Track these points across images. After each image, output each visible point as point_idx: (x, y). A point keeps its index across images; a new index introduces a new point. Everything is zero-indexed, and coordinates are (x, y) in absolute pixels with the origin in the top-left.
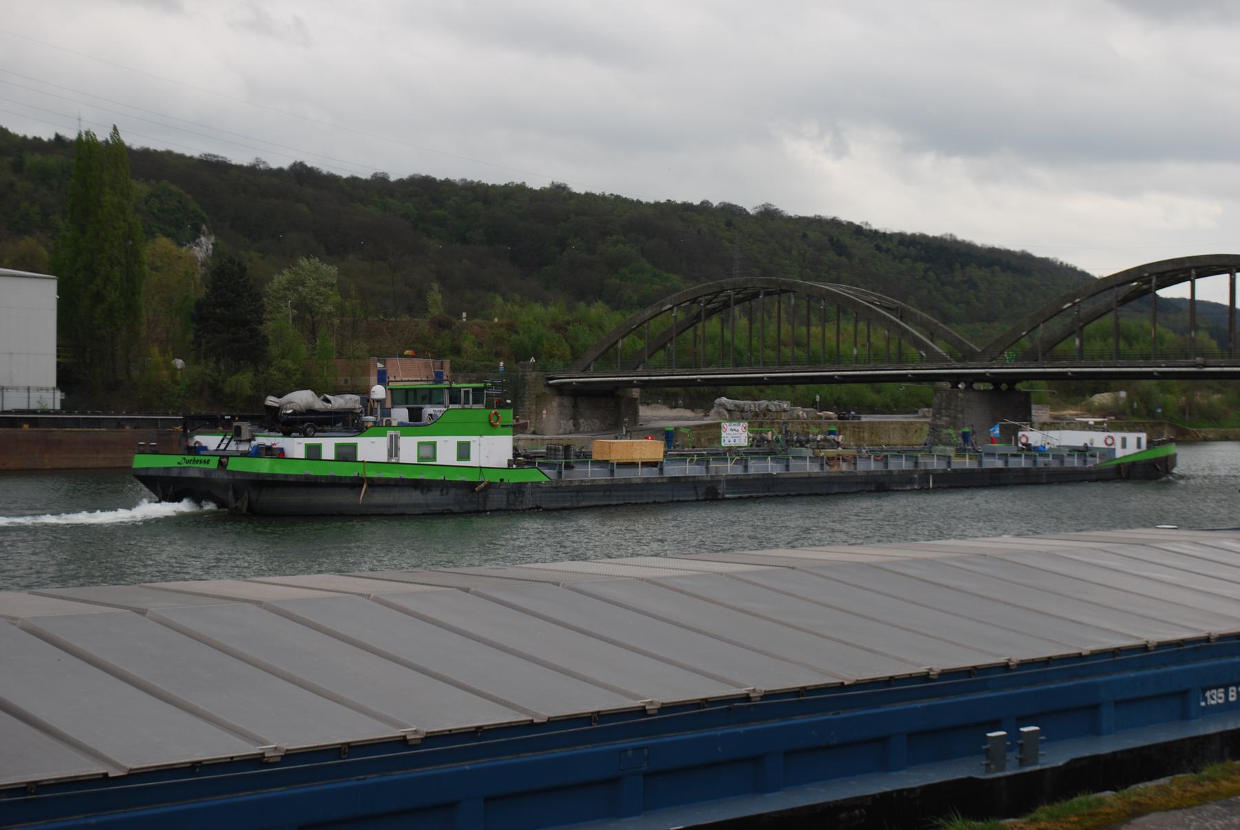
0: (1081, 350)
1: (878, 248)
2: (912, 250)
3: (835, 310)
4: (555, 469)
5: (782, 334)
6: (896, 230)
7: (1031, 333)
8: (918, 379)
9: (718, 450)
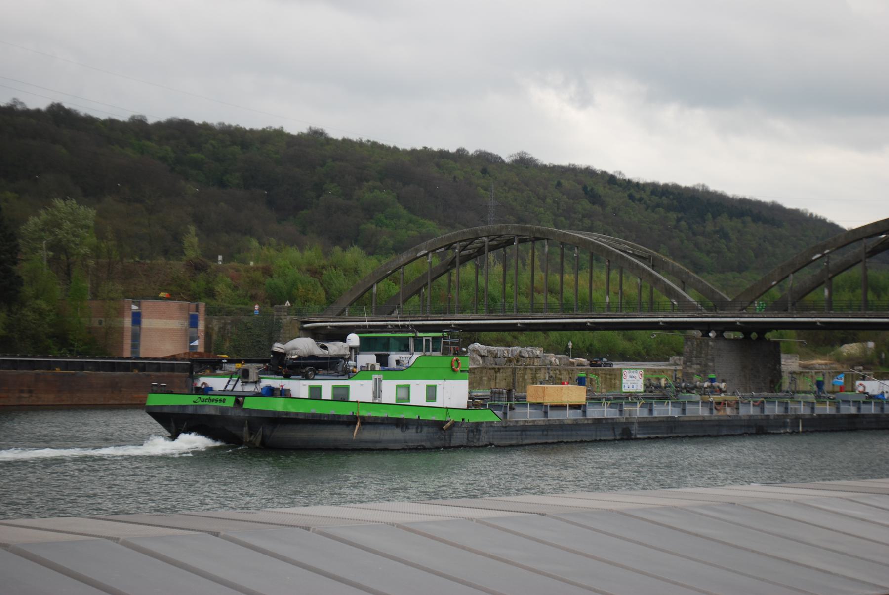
0: (830, 301)
1: (631, 197)
2: (665, 200)
3: (588, 258)
4: (500, 411)
5: (535, 281)
6: (649, 180)
7: (781, 283)
8: (670, 327)
9: (622, 395)
